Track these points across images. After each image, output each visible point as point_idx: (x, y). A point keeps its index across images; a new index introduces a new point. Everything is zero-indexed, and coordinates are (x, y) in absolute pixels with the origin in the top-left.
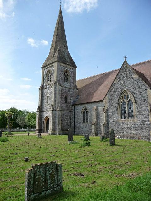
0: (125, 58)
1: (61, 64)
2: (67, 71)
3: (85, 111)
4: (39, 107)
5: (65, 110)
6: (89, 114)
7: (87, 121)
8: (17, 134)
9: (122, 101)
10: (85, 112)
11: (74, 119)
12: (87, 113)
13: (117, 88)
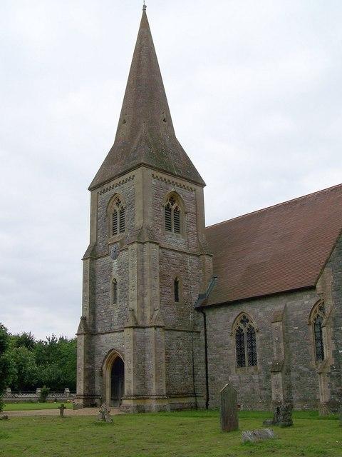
4: (83, 319)
5: (174, 326)
6: (258, 336)
7: (253, 362)
10: (245, 331)
12: (251, 333)
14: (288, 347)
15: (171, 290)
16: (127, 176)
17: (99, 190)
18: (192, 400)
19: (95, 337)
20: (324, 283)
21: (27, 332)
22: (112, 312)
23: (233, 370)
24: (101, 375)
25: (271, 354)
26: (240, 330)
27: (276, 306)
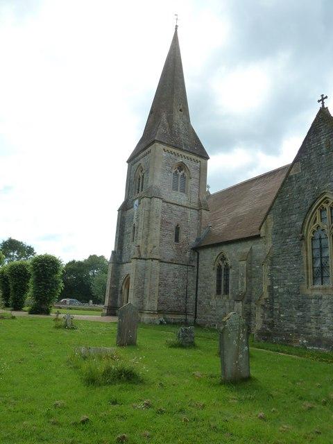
0: (323, 99)
1: (167, 148)
2: (181, 167)
3: (220, 262)
5: (172, 260)
6: (231, 271)
7: (227, 292)
8: (81, 316)
9: (313, 227)
10: (223, 267)
11: (197, 286)
12: (227, 269)
13: (300, 191)
14: (250, 281)
15: (173, 234)
16: (147, 151)
17: (132, 162)
18: (182, 317)
19: (121, 265)
20: (267, 227)
21: (71, 260)
22: (131, 248)
23: (213, 295)
24: (121, 293)
25: (238, 288)
26: (219, 267)
27: (244, 248)
